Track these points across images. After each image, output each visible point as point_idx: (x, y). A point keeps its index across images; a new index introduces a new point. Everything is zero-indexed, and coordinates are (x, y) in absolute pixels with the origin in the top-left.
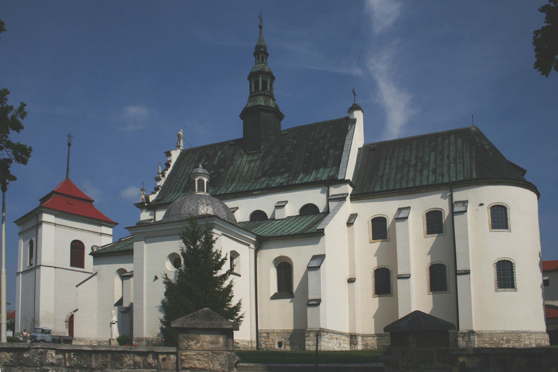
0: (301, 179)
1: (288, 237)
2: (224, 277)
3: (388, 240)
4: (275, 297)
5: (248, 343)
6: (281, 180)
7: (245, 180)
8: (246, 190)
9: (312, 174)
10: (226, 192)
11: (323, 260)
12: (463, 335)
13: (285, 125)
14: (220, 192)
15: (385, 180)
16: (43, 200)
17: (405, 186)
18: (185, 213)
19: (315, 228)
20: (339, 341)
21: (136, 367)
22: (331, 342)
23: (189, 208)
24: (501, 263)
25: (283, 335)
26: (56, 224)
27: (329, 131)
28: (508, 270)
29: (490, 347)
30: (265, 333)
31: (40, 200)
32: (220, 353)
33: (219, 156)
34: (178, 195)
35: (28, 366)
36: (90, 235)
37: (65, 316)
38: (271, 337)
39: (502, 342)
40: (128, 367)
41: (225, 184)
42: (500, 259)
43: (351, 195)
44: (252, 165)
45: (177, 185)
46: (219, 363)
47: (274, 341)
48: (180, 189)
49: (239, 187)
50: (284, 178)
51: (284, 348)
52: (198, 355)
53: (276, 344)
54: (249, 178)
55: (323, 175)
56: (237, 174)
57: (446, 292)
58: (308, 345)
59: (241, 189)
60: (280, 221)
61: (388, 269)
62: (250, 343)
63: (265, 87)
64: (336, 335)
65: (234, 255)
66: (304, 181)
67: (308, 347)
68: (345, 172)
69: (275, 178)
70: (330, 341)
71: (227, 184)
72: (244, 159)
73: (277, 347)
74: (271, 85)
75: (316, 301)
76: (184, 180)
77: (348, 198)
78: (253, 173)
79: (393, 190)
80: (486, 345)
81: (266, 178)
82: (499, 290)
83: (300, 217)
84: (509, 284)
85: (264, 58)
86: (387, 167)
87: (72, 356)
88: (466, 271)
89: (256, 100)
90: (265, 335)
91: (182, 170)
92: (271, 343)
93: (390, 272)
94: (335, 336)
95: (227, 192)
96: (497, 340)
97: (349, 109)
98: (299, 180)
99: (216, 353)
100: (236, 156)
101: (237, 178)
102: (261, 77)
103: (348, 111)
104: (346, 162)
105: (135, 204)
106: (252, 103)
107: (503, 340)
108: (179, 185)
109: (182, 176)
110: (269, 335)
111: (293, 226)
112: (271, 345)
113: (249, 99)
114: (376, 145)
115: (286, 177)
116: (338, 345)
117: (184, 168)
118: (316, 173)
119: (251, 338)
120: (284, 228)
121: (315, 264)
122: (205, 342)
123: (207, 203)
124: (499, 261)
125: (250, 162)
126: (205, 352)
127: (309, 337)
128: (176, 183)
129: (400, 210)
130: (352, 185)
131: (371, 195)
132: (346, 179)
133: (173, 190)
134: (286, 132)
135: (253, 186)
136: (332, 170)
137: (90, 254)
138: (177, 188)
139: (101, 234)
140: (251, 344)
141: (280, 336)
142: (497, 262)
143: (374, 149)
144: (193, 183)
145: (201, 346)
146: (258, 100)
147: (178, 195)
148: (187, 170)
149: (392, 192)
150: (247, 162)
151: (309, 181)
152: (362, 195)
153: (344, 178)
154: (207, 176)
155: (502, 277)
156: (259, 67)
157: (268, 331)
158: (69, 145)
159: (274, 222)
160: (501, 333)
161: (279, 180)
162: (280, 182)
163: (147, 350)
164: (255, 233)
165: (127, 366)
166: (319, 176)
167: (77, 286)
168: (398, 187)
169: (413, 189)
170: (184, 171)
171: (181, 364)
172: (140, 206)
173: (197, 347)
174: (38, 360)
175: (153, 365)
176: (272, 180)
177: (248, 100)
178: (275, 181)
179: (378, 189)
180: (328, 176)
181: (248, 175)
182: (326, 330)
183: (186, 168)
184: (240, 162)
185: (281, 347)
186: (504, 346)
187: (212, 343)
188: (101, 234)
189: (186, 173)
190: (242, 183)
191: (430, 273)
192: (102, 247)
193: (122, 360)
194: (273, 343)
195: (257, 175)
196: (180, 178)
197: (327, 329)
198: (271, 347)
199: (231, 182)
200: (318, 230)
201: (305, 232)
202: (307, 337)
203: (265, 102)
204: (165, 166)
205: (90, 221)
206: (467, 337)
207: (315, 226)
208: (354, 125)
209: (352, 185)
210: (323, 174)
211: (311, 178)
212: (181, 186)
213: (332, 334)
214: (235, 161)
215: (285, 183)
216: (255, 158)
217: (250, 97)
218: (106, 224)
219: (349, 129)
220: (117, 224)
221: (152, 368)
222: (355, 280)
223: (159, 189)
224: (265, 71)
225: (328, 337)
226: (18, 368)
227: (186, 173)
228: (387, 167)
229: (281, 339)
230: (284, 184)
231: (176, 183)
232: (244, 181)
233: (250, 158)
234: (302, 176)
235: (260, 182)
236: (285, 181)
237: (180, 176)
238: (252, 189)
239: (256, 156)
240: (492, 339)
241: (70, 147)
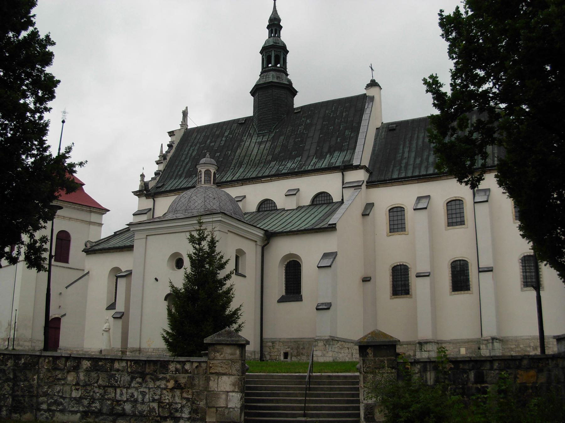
0: (314, 163)
1: (298, 232)
2: (228, 277)
3: (406, 233)
4: (282, 300)
5: (251, 354)
6: (292, 166)
7: (254, 164)
8: (254, 176)
9: (326, 158)
10: (232, 178)
11: (336, 255)
12: (486, 342)
13: (299, 102)
14: (226, 178)
15: (403, 165)
17: (425, 173)
18: (190, 209)
19: (326, 221)
20: (351, 351)
21: (177, 373)
22: (342, 352)
23: (195, 203)
24: (526, 258)
25: (290, 344)
27: (345, 109)
29: (516, 355)
30: (269, 342)
32: (236, 362)
33: (227, 137)
34: (180, 181)
35: (102, 372)
38: (277, 347)
39: (528, 349)
40: (171, 372)
41: (232, 169)
42: (526, 254)
43: (367, 182)
44: (262, 146)
45: (180, 168)
46: (236, 369)
47: (279, 351)
48: (182, 173)
49: (247, 173)
50: (296, 163)
51: (290, 360)
52: (221, 364)
53: (281, 355)
54: (258, 162)
55: (338, 159)
56: (245, 157)
57: (469, 292)
58: (317, 356)
59: (249, 175)
60: (291, 211)
61: (407, 266)
62: (253, 354)
64: (347, 343)
65: (239, 254)
66: (317, 167)
67: (317, 358)
68: (361, 157)
69: (286, 163)
70: (340, 351)
71: (234, 169)
72: (254, 140)
73: (282, 358)
75: (325, 305)
76: (187, 164)
77: (364, 186)
78: (263, 156)
79: (412, 177)
80: (512, 352)
81: (276, 162)
82: (526, 289)
83: (312, 207)
86: (407, 150)
87: (133, 364)
88: (488, 269)
89: (268, 77)
90: (270, 344)
91: (186, 153)
92: (276, 354)
93: (409, 270)
94: (346, 345)
95: (233, 179)
96: (524, 348)
97: (366, 85)
98: (312, 166)
99: (233, 362)
100: (245, 136)
101: (245, 161)
102: (274, 51)
103: (365, 87)
104: (363, 145)
105: (133, 192)
106: (264, 79)
107: (530, 347)
108: (182, 169)
109: (185, 159)
110: (274, 344)
111: (304, 218)
112: (276, 356)
113: (261, 74)
114: (395, 125)
115: (298, 161)
116: (350, 356)
117: (187, 149)
118: (330, 157)
120: (294, 222)
121: (326, 262)
122: (226, 353)
123: (213, 197)
124: (524, 257)
125: (260, 143)
126: (226, 361)
127: (317, 347)
128: (179, 167)
129: (419, 199)
130: (368, 171)
131: (388, 182)
132: (361, 165)
133: (175, 174)
134: (299, 110)
135: (263, 171)
136: (347, 154)
137: (82, 251)
138: (180, 173)
140: (255, 355)
141: (286, 345)
142: (522, 257)
143: (392, 130)
144: (199, 174)
145: (224, 357)
146: (270, 76)
147: (180, 181)
148: (190, 152)
149: (410, 179)
150: (256, 144)
151: (323, 167)
152: (379, 183)
153: (359, 164)
154: (215, 166)
157: (273, 340)
158: (63, 122)
159: (284, 212)
160: (528, 339)
161: (290, 165)
162: (291, 168)
163: (185, 360)
164: (261, 227)
165: (171, 371)
166: (333, 161)
167: (67, 288)
168: (417, 174)
169: (433, 176)
170: (188, 153)
171: (210, 370)
172: (138, 193)
173: (221, 358)
174: (108, 367)
175: (189, 371)
176: (283, 165)
177: (260, 76)
178: (286, 165)
179: (395, 176)
180: (343, 161)
181: (257, 159)
182: (336, 339)
183: (189, 150)
184: (249, 143)
185: (287, 359)
186: (531, 354)
187: (231, 354)
189: (189, 155)
190: (251, 168)
191: (452, 271)
192: (95, 242)
193: (167, 367)
194: (279, 354)
195: (266, 158)
196: (184, 161)
197: (337, 338)
198: (276, 358)
199: (238, 167)
200: (330, 225)
201: (316, 227)
202: (315, 346)
204: (168, 147)
205: (80, 208)
206: (491, 344)
207: (327, 220)
208: (372, 103)
209: (368, 171)
210: (338, 159)
211: (325, 162)
212: (184, 170)
213: (343, 343)
214: (244, 143)
215: (297, 168)
216: (265, 139)
217: (262, 73)
218: (96, 211)
220: (109, 211)
221: (188, 373)
222: (371, 279)
223: (160, 174)
224: (278, 45)
225: (338, 346)
226: (95, 372)
227: (189, 155)
228: (407, 150)
229: (288, 349)
230: (296, 170)
231: (179, 167)
232: (253, 165)
233: (259, 140)
234: (315, 160)
235: (270, 167)
236: (297, 166)
237: (183, 159)
238: (260, 175)
239: (267, 137)
240: (518, 346)
241: (64, 124)
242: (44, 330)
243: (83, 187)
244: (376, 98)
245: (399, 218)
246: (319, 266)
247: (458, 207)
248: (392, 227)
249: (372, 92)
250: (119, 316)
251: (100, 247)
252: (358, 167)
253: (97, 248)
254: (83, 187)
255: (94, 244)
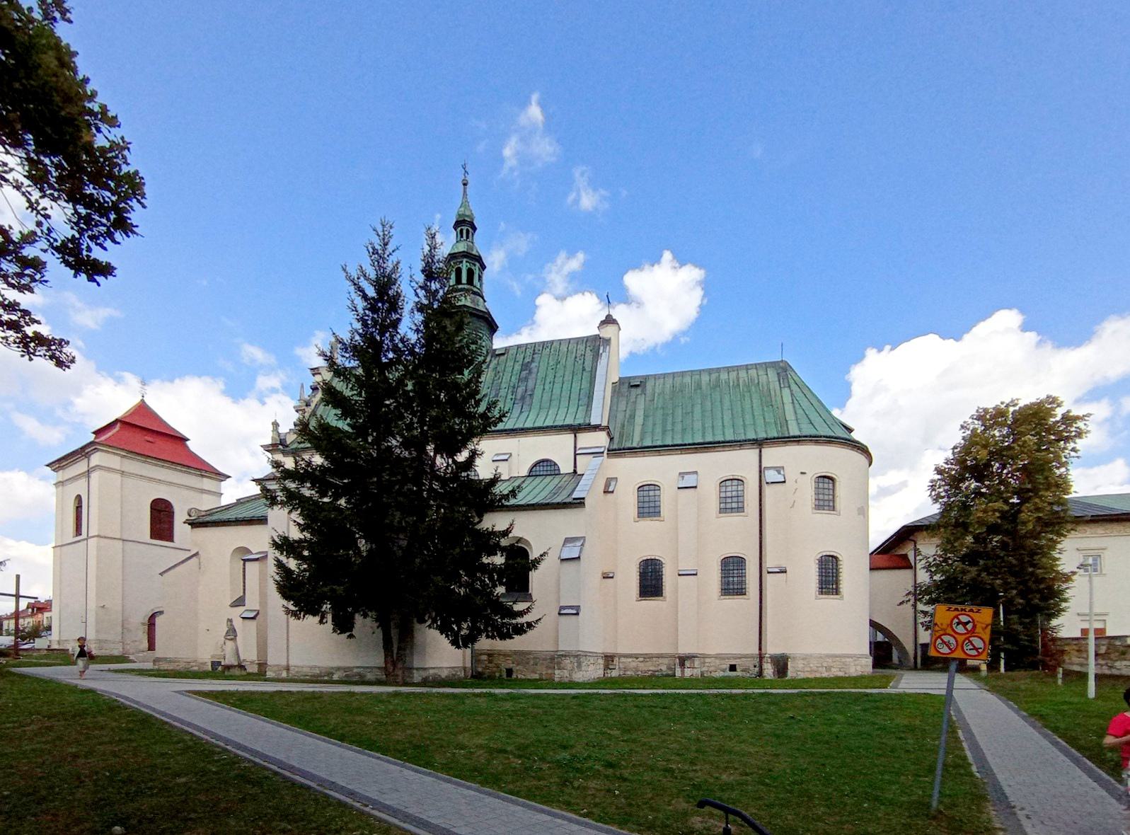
3: (637, 519)
16: (98, 433)
26: (123, 473)
28: (832, 569)
31: (94, 433)
36: (185, 492)
37: (141, 617)
63: (470, 281)
74: (480, 277)
84: (833, 589)
85: (470, 234)
119: (464, 663)
137: (185, 523)
139: (203, 491)
155: (824, 579)
156: (462, 247)
167: (18, 577)
188: (203, 491)
200: (574, 499)
203: (473, 301)
219: (601, 351)
220: (229, 477)
242: (851, 391)
243: (188, 443)
244: (613, 342)
245: (723, 489)
246: (564, 556)
247: (740, 488)
248: (641, 510)
249: (608, 332)
250: (252, 615)
251: (215, 518)
252: (597, 428)
253: (208, 519)
254: (188, 443)
255: (203, 513)
